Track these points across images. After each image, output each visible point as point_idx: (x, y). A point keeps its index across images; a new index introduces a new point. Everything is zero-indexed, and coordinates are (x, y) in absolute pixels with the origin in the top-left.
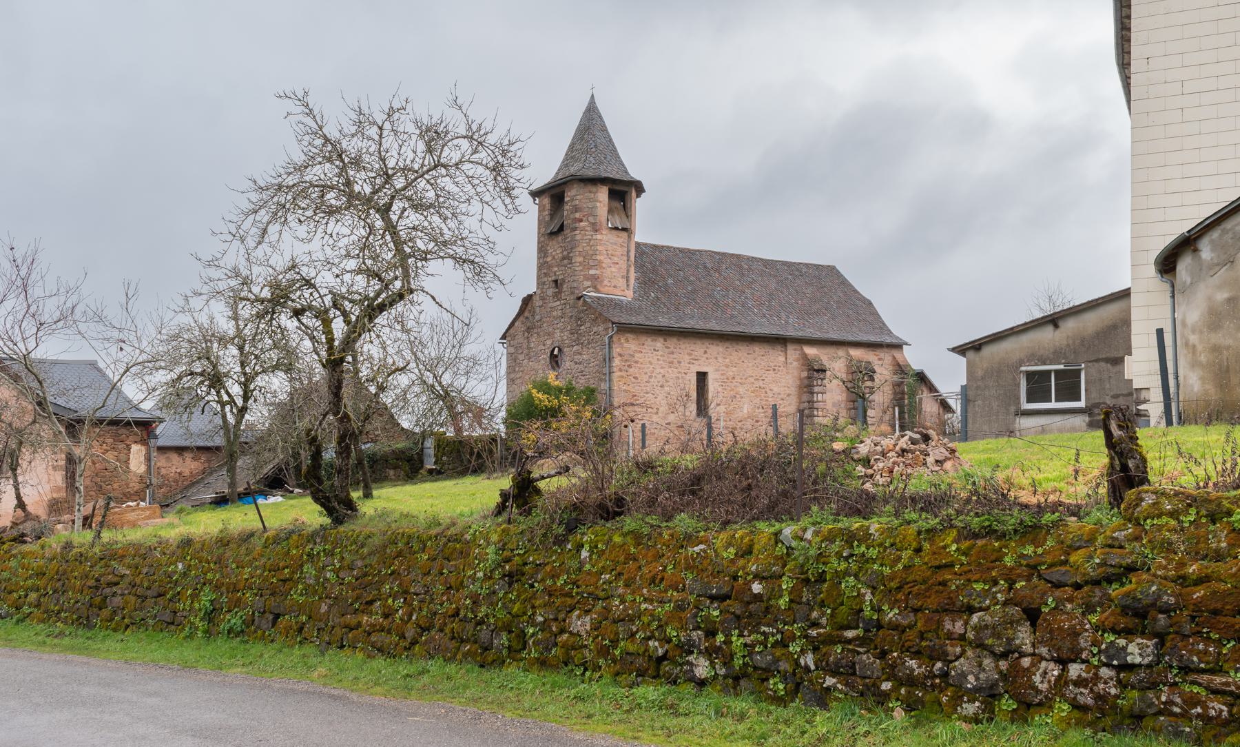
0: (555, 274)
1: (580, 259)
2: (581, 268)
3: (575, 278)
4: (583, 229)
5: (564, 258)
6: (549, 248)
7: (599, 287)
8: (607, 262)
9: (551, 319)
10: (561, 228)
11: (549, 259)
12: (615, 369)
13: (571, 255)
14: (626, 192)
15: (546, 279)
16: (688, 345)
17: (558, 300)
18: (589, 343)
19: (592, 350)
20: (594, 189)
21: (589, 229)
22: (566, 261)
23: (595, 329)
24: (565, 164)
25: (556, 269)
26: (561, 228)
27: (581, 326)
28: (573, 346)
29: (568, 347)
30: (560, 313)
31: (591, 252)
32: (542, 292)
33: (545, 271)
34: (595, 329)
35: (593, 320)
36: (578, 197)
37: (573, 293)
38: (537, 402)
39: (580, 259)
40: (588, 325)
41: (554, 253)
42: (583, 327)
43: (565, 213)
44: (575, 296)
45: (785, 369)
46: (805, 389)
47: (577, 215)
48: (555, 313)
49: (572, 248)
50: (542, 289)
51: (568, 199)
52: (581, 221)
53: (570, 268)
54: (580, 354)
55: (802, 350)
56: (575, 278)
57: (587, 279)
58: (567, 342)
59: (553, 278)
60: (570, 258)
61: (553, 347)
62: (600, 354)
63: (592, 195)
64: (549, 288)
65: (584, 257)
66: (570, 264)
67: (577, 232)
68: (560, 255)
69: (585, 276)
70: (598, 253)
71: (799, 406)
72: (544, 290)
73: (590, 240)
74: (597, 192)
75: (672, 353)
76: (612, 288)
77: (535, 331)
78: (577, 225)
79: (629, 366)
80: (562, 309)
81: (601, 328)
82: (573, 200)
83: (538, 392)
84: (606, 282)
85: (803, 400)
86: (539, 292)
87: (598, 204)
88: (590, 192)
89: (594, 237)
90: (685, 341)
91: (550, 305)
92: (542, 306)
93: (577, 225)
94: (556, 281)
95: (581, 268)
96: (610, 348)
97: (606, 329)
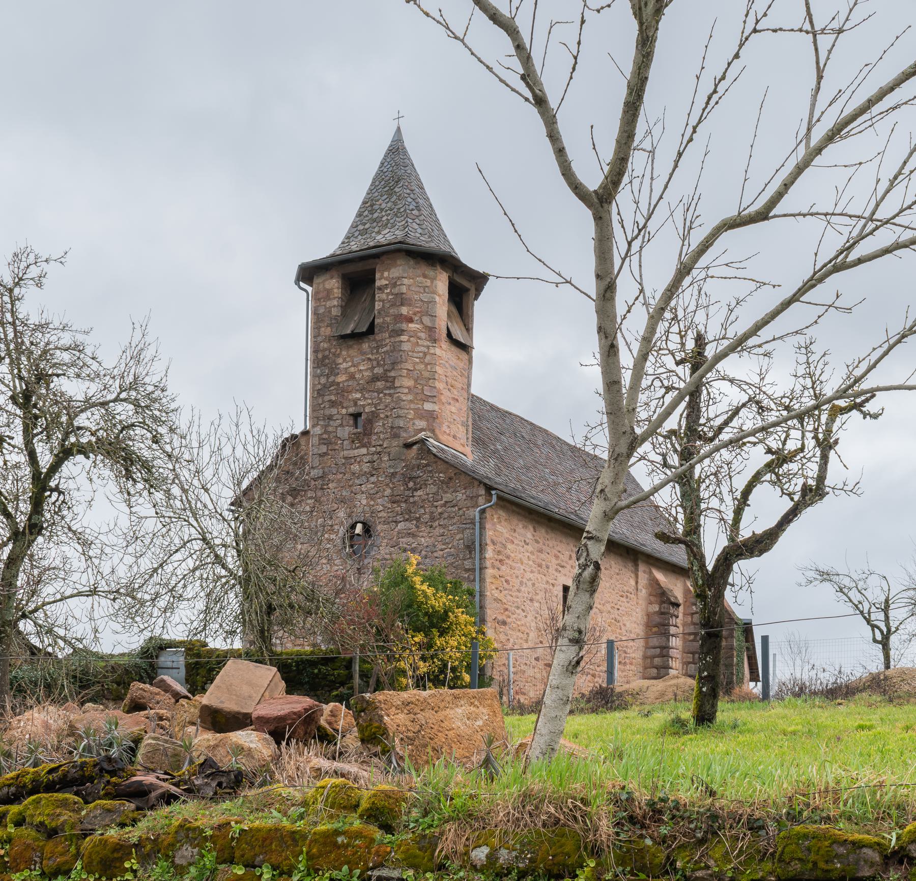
0: (356, 404)
1: (410, 383)
2: (410, 397)
3: (401, 412)
4: (414, 334)
5: (375, 379)
6: (340, 360)
7: (437, 431)
8: (446, 395)
9: (347, 476)
10: (371, 330)
11: (341, 378)
12: (488, 564)
13: (392, 374)
14: (467, 290)
15: (334, 411)
16: (555, 543)
17: (363, 446)
18: (433, 519)
20: (430, 273)
21: (423, 335)
23: (448, 497)
24: (360, 226)
25: (358, 395)
26: (371, 330)
28: (397, 522)
29: (386, 522)
30: (366, 467)
31: (426, 374)
32: (326, 432)
33: (333, 398)
34: (448, 497)
35: (443, 482)
36: (406, 281)
37: (396, 436)
38: (421, 598)
39: (410, 383)
40: (432, 489)
41: (352, 369)
42: (419, 493)
43: (378, 306)
45: (635, 597)
46: (655, 629)
47: (404, 310)
48: (355, 468)
50: (326, 426)
51: (384, 282)
52: (411, 320)
53: (390, 395)
54: (414, 535)
55: (651, 573)
57: (421, 418)
58: (383, 514)
59: (352, 410)
60: (391, 382)
61: (350, 522)
62: (458, 537)
63: (428, 283)
65: (416, 381)
66: (389, 388)
67: (404, 338)
68: (366, 374)
69: (416, 410)
71: (645, 652)
73: (425, 354)
75: (541, 551)
78: (404, 326)
79: (501, 561)
81: (460, 496)
82: (395, 285)
83: (422, 583)
84: (445, 428)
85: (651, 644)
86: (318, 430)
87: (437, 299)
88: (425, 276)
89: (432, 351)
90: (553, 535)
92: (325, 454)
93: (404, 326)
94: (356, 416)
95: (410, 397)
96: (482, 528)
97: (474, 498)
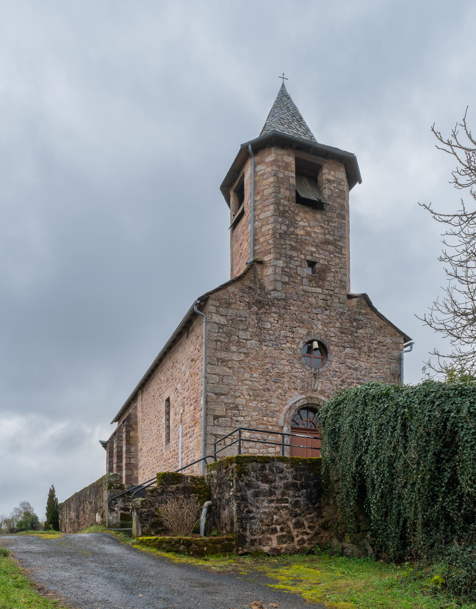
18: (370, 351)
19: (373, 360)
23: (380, 339)
34: (380, 339)
42: (361, 331)
54: (357, 359)
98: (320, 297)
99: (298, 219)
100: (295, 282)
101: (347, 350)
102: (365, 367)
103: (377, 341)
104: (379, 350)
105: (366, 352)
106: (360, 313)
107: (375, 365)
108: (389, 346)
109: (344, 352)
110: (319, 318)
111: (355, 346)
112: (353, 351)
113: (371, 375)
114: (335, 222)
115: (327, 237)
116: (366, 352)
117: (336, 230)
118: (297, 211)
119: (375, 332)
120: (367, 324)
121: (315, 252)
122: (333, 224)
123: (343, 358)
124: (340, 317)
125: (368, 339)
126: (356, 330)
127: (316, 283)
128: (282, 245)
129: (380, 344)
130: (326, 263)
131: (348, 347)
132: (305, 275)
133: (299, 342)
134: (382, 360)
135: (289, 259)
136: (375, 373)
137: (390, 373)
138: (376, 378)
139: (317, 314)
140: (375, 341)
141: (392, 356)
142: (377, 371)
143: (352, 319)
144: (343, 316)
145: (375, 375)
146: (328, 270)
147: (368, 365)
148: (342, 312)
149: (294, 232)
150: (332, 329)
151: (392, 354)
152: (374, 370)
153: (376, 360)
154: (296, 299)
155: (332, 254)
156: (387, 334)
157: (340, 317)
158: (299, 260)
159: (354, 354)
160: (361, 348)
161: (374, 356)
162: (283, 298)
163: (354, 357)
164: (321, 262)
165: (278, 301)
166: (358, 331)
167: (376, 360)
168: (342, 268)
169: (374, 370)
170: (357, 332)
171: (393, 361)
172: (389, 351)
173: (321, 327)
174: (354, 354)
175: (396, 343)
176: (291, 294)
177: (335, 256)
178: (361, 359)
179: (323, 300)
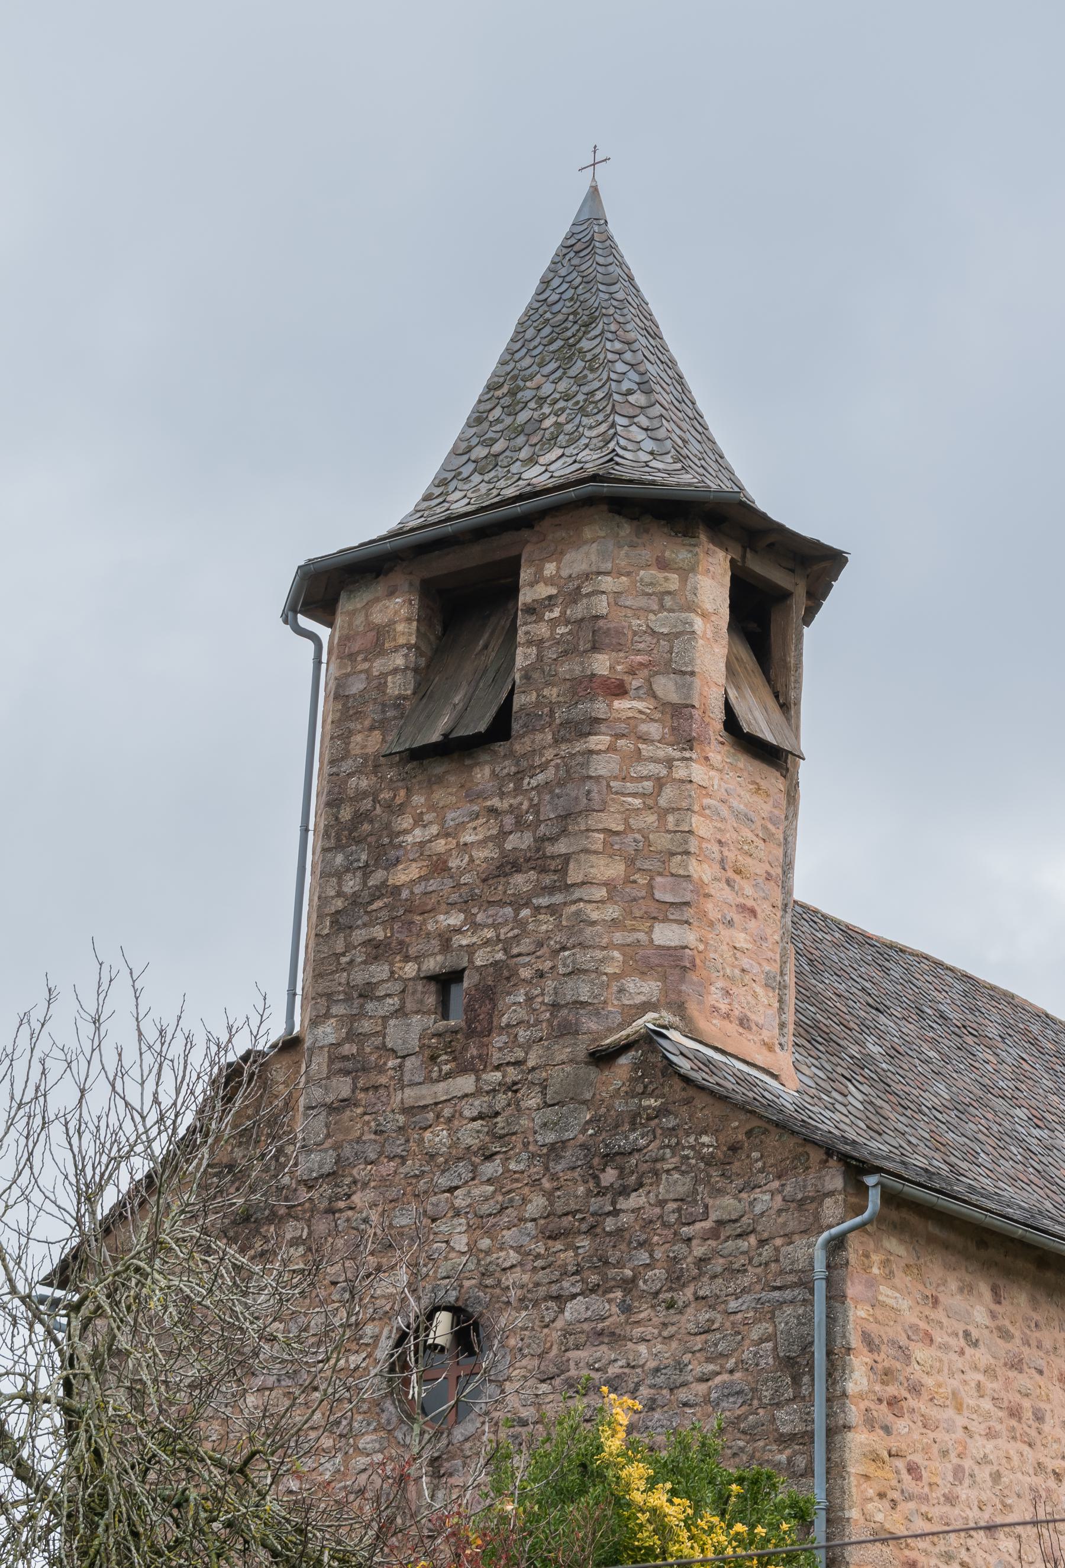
0: (446, 945)
1: (613, 870)
2: (612, 911)
3: (584, 958)
4: (630, 730)
9: (412, 1166)
11: (405, 874)
12: (854, 1413)
13: (561, 847)
14: (783, 596)
15: (379, 971)
17: (463, 1070)
18: (676, 1280)
19: (693, 1318)
20: (681, 555)
21: (654, 730)
22: (522, 882)
23: (725, 1205)
25: (455, 919)
27: (625, 1191)
28: (560, 1300)
30: (470, 1135)
31: (662, 841)
32: (351, 1036)
33: (378, 933)
34: (725, 1205)
35: (709, 1161)
36: (607, 583)
37: (567, 1031)
39: (613, 870)
42: (635, 1200)
43: (523, 657)
44: (582, 1047)
47: (601, 664)
48: (438, 1137)
49: (566, 817)
50: (353, 1018)
51: (544, 591)
52: (620, 690)
53: (552, 909)
54: (614, 1338)
56: (584, 958)
57: (645, 969)
59: (433, 964)
63: (673, 581)
64: (400, 1012)
65: (630, 862)
66: (551, 890)
67: (599, 741)
70: (693, 846)
72: (366, 1026)
73: (660, 783)
74: (693, 569)
76: (732, 1028)
77: (292, 1229)
78: (600, 708)
80: (487, 1116)
83: (652, 1483)
86: (328, 1033)
87: (698, 624)
88: (663, 565)
89: (680, 773)
91: (410, 1095)
93: (600, 708)
95: (612, 911)
96: (835, 1297)
98: (467, 1113)
99: (405, 826)
100: (376, 1088)
101: (574, 1310)
102: (652, 1364)
103: (708, 1224)
104: (718, 1265)
105: (656, 1294)
106: (634, 1120)
107: (698, 1342)
108: (765, 1228)
109: (559, 1324)
110: (458, 1203)
111: (605, 1278)
112: (598, 1304)
113: (683, 1395)
114: (543, 767)
115: (512, 842)
116: (656, 1294)
117: (547, 797)
118: (402, 793)
119: (696, 1181)
120: (663, 1159)
121: (458, 931)
122: (541, 778)
123: (555, 1351)
124: (547, 1169)
125: (666, 1225)
126: (614, 1203)
127: (454, 1059)
128: (338, 956)
129: (728, 1230)
130: (500, 956)
131: (574, 1296)
132: (414, 1044)
133: (376, 1338)
134: (733, 1305)
135: (357, 1002)
136: (704, 1379)
137: (777, 1357)
138: (707, 1400)
139: (451, 1190)
140: (698, 1226)
141: (782, 1272)
142: (711, 1367)
143: (596, 1161)
144: (559, 1158)
145: (702, 1388)
146: (508, 979)
147: (667, 1352)
148: (552, 1147)
149: (384, 883)
150: (509, 1236)
151: (785, 1263)
152: (699, 1367)
153: (704, 1316)
154: (373, 1156)
155: (527, 905)
156: (761, 1171)
157: (547, 1169)
158: (398, 987)
159: (603, 1319)
160: (634, 1280)
161: (697, 1299)
162: (326, 1169)
163: (601, 1334)
164: (481, 959)
165: (310, 1188)
166: (623, 1204)
167: (704, 1316)
168: (564, 948)
169: (699, 1367)
170: (615, 1213)
171: (788, 1294)
172: (767, 1252)
173: (464, 1239)
174: (603, 1319)
175: (801, 1203)
176: (358, 1141)
177: (537, 909)
178: (637, 1331)
179: (481, 1117)
